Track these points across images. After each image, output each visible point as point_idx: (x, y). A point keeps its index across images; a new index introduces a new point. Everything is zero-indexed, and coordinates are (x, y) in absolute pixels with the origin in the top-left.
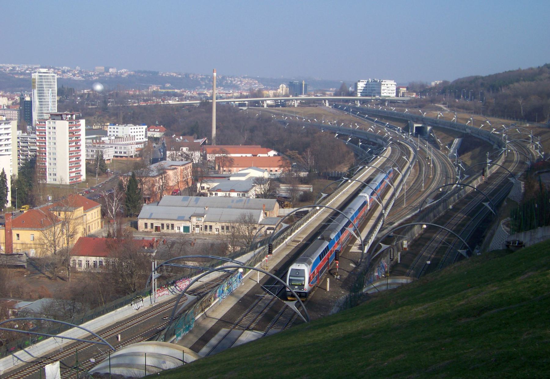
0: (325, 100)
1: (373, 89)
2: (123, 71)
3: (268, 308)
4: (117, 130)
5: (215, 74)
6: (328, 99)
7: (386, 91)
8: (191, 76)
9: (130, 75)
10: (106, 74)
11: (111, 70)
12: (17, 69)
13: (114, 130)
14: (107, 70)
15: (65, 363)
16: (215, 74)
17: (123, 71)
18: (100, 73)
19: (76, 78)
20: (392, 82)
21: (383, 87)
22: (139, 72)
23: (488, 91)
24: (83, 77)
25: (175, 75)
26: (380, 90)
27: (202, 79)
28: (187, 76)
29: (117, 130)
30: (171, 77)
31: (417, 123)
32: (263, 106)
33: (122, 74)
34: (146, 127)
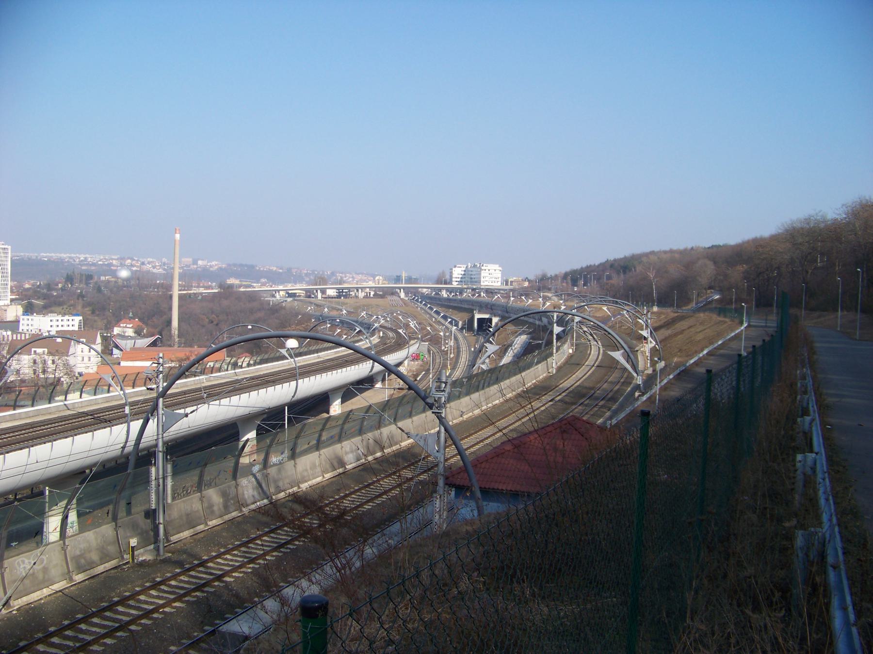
0: (400, 288)
1: (471, 277)
2: (214, 263)
3: (527, 418)
4: (51, 323)
5: (178, 236)
6: (404, 288)
7: (487, 279)
8: (294, 271)
9: (221, 269)
10: (192, 266)
11: (200, 262)
12: (89, 259)
13: (68, 323)
14: (195, 262)
15: (453, 433)
16: (178, 236)
17: (214, 263)
18: (187, 266)
19: (155, 271)
20: (497, 267)
21: (483, 274)
22: (235, 265)
23: (618, 273)
24: (164, 269)
25: (275, 269)
26: (480, 278)
27: (306, 275)
28: (289, 270)
29: (51, 323)
30: (270, 271)
31: (480, 312)
32: (316, 297)
33: (211, 266)
34: (81, 318)
